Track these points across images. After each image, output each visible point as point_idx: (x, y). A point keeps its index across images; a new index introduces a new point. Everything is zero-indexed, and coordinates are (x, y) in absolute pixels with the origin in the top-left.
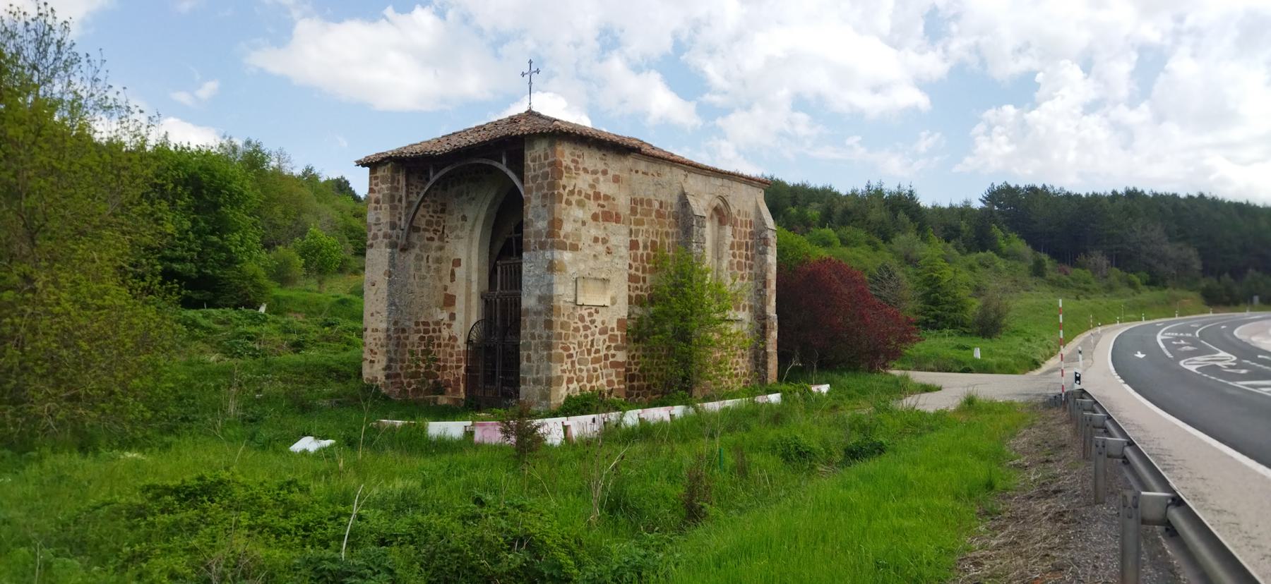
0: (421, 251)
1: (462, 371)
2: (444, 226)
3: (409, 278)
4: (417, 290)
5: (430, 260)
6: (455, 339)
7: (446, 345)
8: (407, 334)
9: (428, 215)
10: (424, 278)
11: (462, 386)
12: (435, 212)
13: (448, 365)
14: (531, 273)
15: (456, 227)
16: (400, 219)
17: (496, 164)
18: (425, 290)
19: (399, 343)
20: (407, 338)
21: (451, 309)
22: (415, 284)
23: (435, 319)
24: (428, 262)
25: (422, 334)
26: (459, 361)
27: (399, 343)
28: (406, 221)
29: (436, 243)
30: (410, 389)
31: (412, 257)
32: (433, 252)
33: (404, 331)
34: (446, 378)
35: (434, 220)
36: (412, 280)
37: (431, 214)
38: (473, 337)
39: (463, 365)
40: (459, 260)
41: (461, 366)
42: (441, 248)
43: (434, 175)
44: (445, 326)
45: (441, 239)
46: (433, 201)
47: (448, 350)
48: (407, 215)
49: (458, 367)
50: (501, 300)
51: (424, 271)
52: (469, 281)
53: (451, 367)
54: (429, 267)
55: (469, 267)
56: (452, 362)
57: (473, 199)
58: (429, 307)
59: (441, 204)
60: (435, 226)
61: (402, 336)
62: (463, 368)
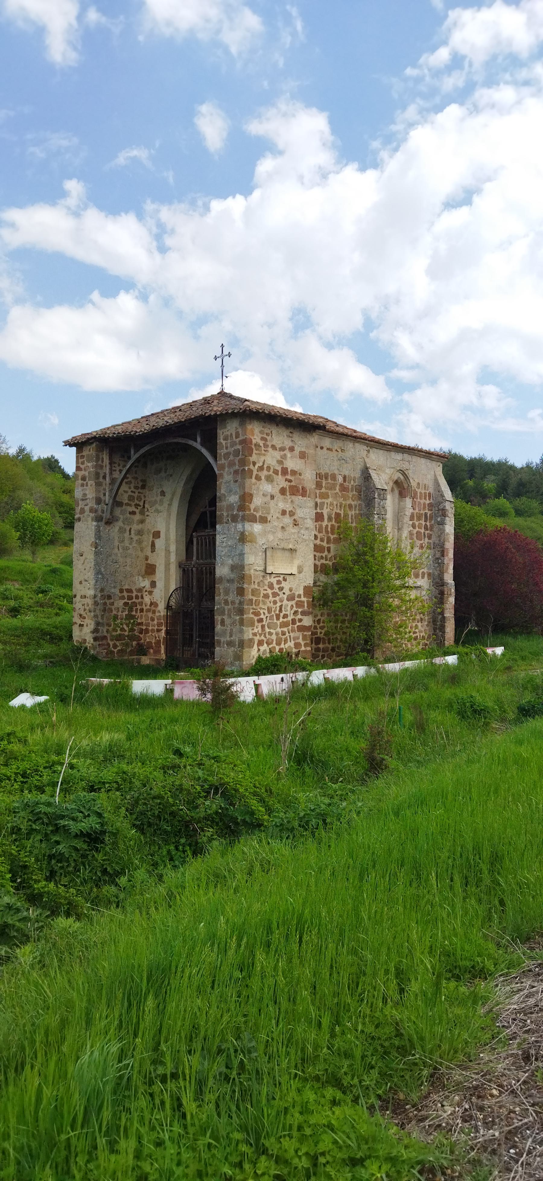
0: (124, 524)
1: (163, 634)
2: (144, 501)
4: (121, 560)
5: (132, 532)
6: (156, 605)
7: (148, 611)
8: (112, 601)
10: (126, 549)
13: (150, 628)
14: (224, 544)
15: (156, 502)
16: (105, 495)
18: (128, 560)
21: (152, 578)
23: (137, 587)
24: (130, 534)
25: (126, 600)
26: (159, 624)
28: (110, 496)
29: (137, 517)
30: (116, 650)
31: (117, 529)
34: (148, 640)
36: (116, 550)
37: (133, 489)
38: (173, 603)
39: (164, 628)
40: (159, 532)
42: (142, 522)
44: (147, 593)
45: (142, 513)
47: (150, 615)
48: (111, 491)
49: (159, 631)
51: (127, 543)
52: (168, 551)
53: (153, 631)
54: (131, 539)
55: (167, 539)
58: (132, 576)
61: (108, 602)
62: (163, 631)
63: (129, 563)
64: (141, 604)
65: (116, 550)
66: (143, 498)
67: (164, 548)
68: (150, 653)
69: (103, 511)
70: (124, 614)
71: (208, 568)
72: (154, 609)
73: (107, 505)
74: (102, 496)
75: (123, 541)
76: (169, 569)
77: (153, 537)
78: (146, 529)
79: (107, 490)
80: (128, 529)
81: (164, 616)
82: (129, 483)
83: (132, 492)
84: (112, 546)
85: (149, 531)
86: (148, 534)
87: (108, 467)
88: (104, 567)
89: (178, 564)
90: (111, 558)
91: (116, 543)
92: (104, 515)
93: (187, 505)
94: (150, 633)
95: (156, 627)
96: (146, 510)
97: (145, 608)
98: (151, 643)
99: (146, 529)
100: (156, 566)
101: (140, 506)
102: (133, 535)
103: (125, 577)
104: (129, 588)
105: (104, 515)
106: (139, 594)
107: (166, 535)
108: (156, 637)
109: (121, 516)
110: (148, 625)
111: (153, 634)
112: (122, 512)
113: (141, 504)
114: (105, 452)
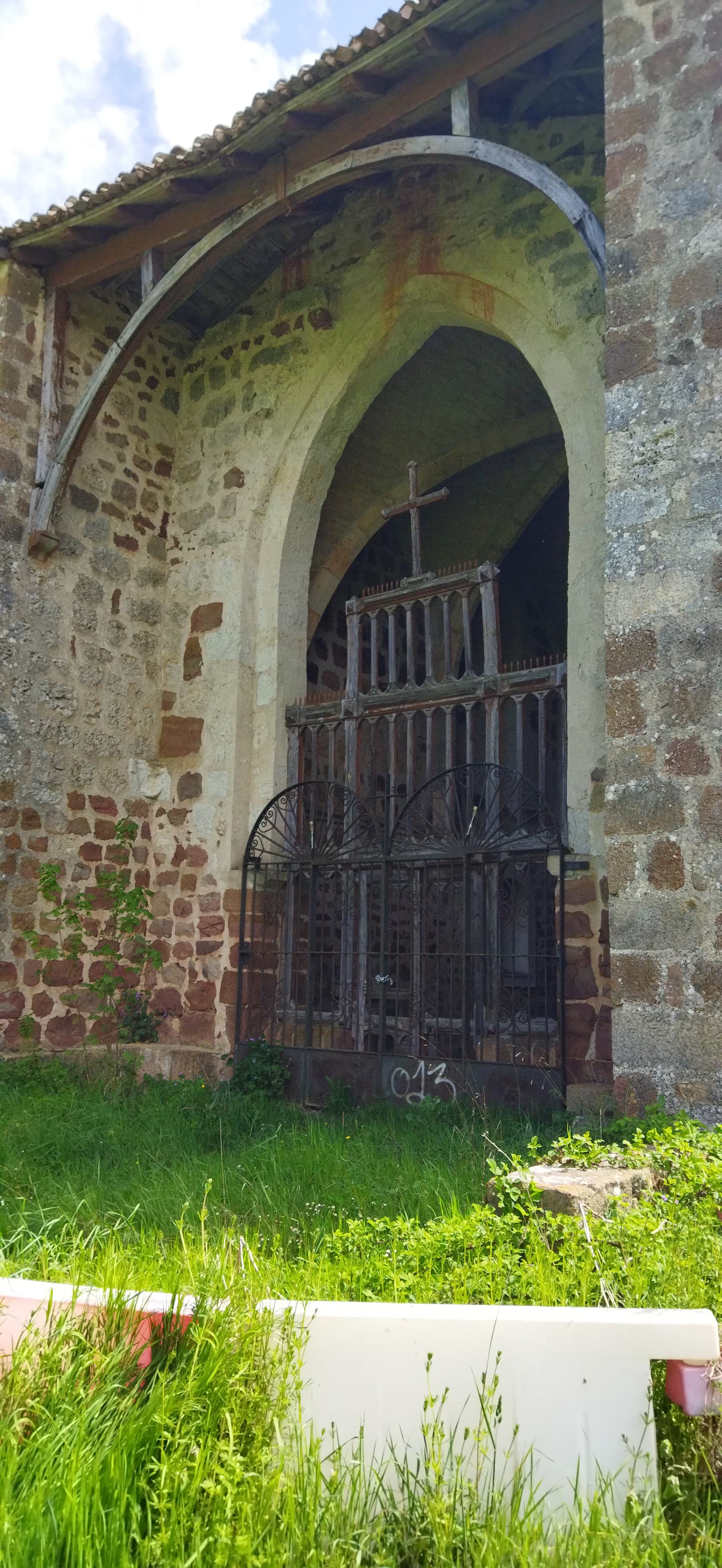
0: (96, 570)
1: (223, 960)
2: (166, 516)
3: (55, 646)
4: (80, 691)
5: (123, 606)
6: (198, 857)
7: (166, 879)
8: (42, 833)
9: (120, 467)
10: (100, 657)
11: (221, 1010)
12: (142, 464)
13: (173, 941)
14: (665, 466)
15: (208, 512)
16: (33, 452)
17: (435, 144)
18: (106, 697)
19: (12, 859)
20: (42, 845)
21: (187, 765)
22: (75, 673)
23: (132, 794)
24: (115, 611)
25: (90, 838)
26: (211, 926)
27: (12, 859)
28: (53, 457)
29: (141, 560)
30: (44, 1022)
31: (69, 583)
32: (132, 584)
33: (31, 819)
34: (162, 985)
35: (140, 487)
36: (64, 656)
37: (130, 465)
38: (265, 846)
39: (227, 941)
40: (217, 608)
41: (218, 945)
42: (156, 579)
43: (155, 283)
44: (164, 819)
45: (157, 550)
46: (135, 430)
47: (174, 893)
48: (55, 439)
49: (206, 949)
50: (362, 722)
51: (102, 638)
52: (249, 672)
53: (182, 950)
54: (119, 627)
55: (248, 629)
56: (189, 933)
57: (268, 414)
58: (116, 754)
59: (161, 447)
60: (139, 508)
61: (26, 836)
62: (225, 952)
63: (106, 710)
64: (142, 855)
65: (64, 656)
66: (161, 503)
67: (234, 655)
68: (167, 1031)
69: (23, 507)
70: (82, 886)
71: (409, 715)
72: (189, 871)
73: (41, 485)
74: (23, 454)
75: (90, 628)
76: (251, 732)
77: (194, 628)
78: (168, 605)
79: (44, 436)
80: (109, 590)
81: (228, 893)
82: (134, 377)
83: (127, 472)
84: (50, 639)
85: (178, 610)
86: (175, 618)
87: (51, 355)
88: (18, 708)
89: (282, 713)
90: (41, 678)
91: (67, 630)
92: (28, 521)
93: (317, 520)
94: (172, 960)
95: (197, 937)
96: (170, 543)
97: (154, 873)
98: (174, 992)
99: (168, 605)
100: (201, 722)
101: (152, 527)
102: (124, 617)
103: (89, 755)
104: (105, 795)
105: (28, 521)
106: (138, 821)
107: (243, 612)
108: (193, 974)
109: (88, 543)
110: (164, 929)
111: (185, 964)
112: (96, 532)
113: (157, 520)
114: (40, 310)
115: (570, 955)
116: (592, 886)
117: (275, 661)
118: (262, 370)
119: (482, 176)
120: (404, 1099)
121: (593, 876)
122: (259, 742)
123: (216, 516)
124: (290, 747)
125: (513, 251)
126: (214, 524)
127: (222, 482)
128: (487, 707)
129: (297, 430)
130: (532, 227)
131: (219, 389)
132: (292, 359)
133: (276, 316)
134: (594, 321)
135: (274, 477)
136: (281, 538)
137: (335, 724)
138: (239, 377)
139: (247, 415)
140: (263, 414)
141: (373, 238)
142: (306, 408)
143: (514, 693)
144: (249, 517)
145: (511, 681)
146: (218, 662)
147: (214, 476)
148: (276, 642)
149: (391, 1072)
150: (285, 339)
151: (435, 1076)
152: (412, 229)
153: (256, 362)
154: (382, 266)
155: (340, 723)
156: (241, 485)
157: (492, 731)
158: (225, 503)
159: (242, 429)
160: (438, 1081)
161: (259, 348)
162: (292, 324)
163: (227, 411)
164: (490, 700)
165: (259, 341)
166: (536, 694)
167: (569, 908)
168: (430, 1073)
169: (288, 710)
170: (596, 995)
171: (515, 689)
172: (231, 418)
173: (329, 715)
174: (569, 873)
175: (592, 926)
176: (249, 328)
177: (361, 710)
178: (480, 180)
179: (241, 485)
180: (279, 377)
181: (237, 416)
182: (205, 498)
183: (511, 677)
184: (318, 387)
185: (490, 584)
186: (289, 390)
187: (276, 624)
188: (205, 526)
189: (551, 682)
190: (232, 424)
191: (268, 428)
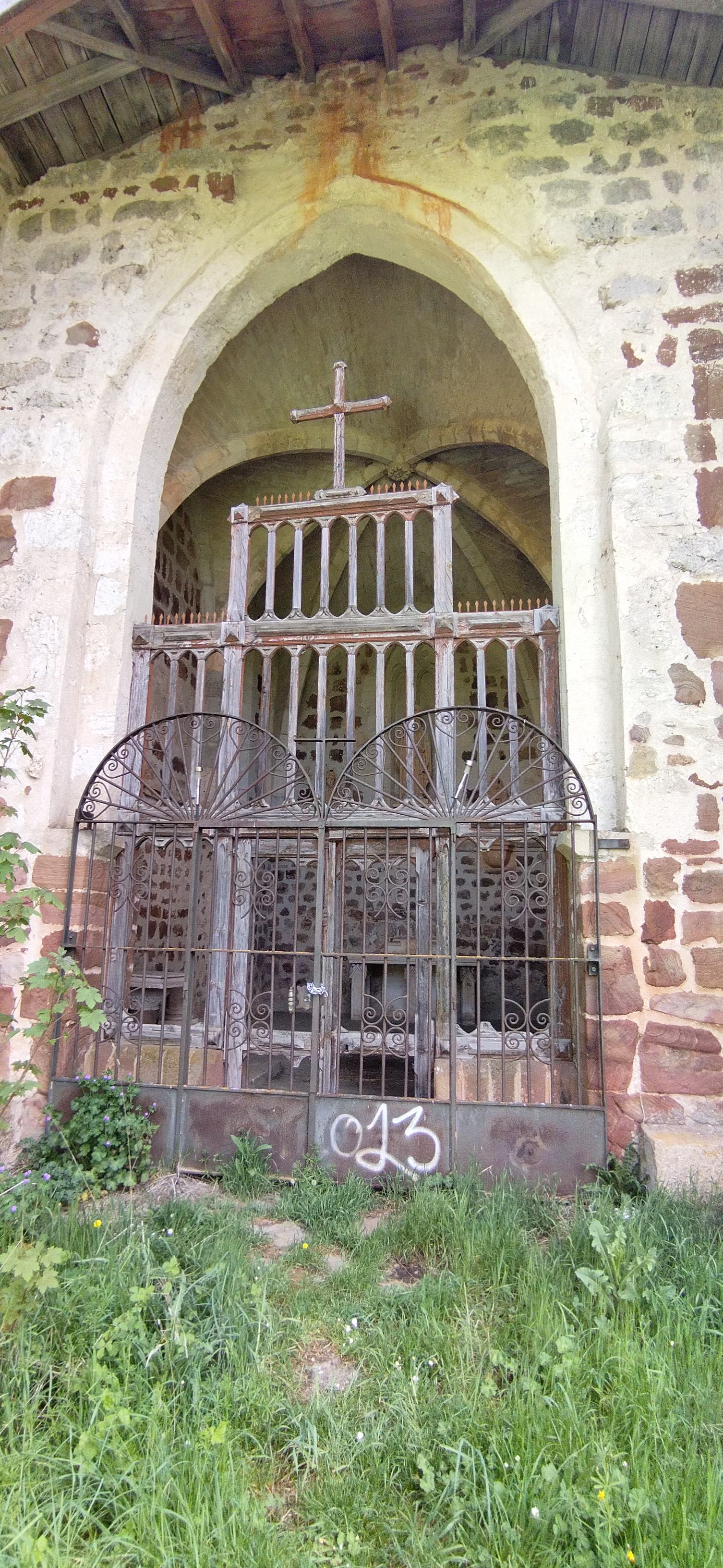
15: (39, 367)
67: (70, 542)
115: (604, 959)
116: (632, 870)
117: (127, 563)
118: (132, 223)
119: (436, 97)
120: (352, 1161)
121: (635, 858)
122: (94, 662)
123: (51, 374)
124: (135, 675)
125: (487, 168)
126: (47, 383)
127: (65, 336)
128: (437, 648)
129: (174, 305)
130: (513, 146)
131: (66, 232)
132: (180, 217)
133: (159, 170)
134: (595, 250)
135: (139, 350)
136: (145, 420)
137: (208, 651)
138: (97, 225)
139: (107, 268)
140: (133, 270)
141: (290, 129)
142: (188, 283)
143: (474, 636)
144: (102, 386)
145: (473, 622)
146: (43, 550)
147: (50, 328)
148: (130, 540)
149: (331, 1120)
150: (168, 196)
151: (404, 1125)
152: (345, 129)
153: (124, 212)
154: (300, 159)
155: (216, 651)
156: (94, 344)
157: (445, 678)
158: (68, 361)
159: (100, 282)
160: (410, 1132)
161: (130, 199)
162: (183, 180)
163: (76, 258)
164: (442, 641)
165: (131, 191)
166: (504, 640)
167: (604, 899)
168: (396, 1121)
169: (136, 628)
170: (640, 1009)
171: (477, 631)
172: (81, 267)
173: (201, 639)
174: (602, 853)
175: (632, 920)
176: (116, 176)
177: (251, 638)
178: (433, 100)
179: (94, 344)
180: (160, 235)
181: (92, 265)
182: (34, 351)
183: (472, 618)
184: (207, 263)
185: (448, 509)
186: (169, 255)
187: (130, 518)
188: (33, 383)
189: (525, 629)
190: (84, 274)
191: (137, 286)
